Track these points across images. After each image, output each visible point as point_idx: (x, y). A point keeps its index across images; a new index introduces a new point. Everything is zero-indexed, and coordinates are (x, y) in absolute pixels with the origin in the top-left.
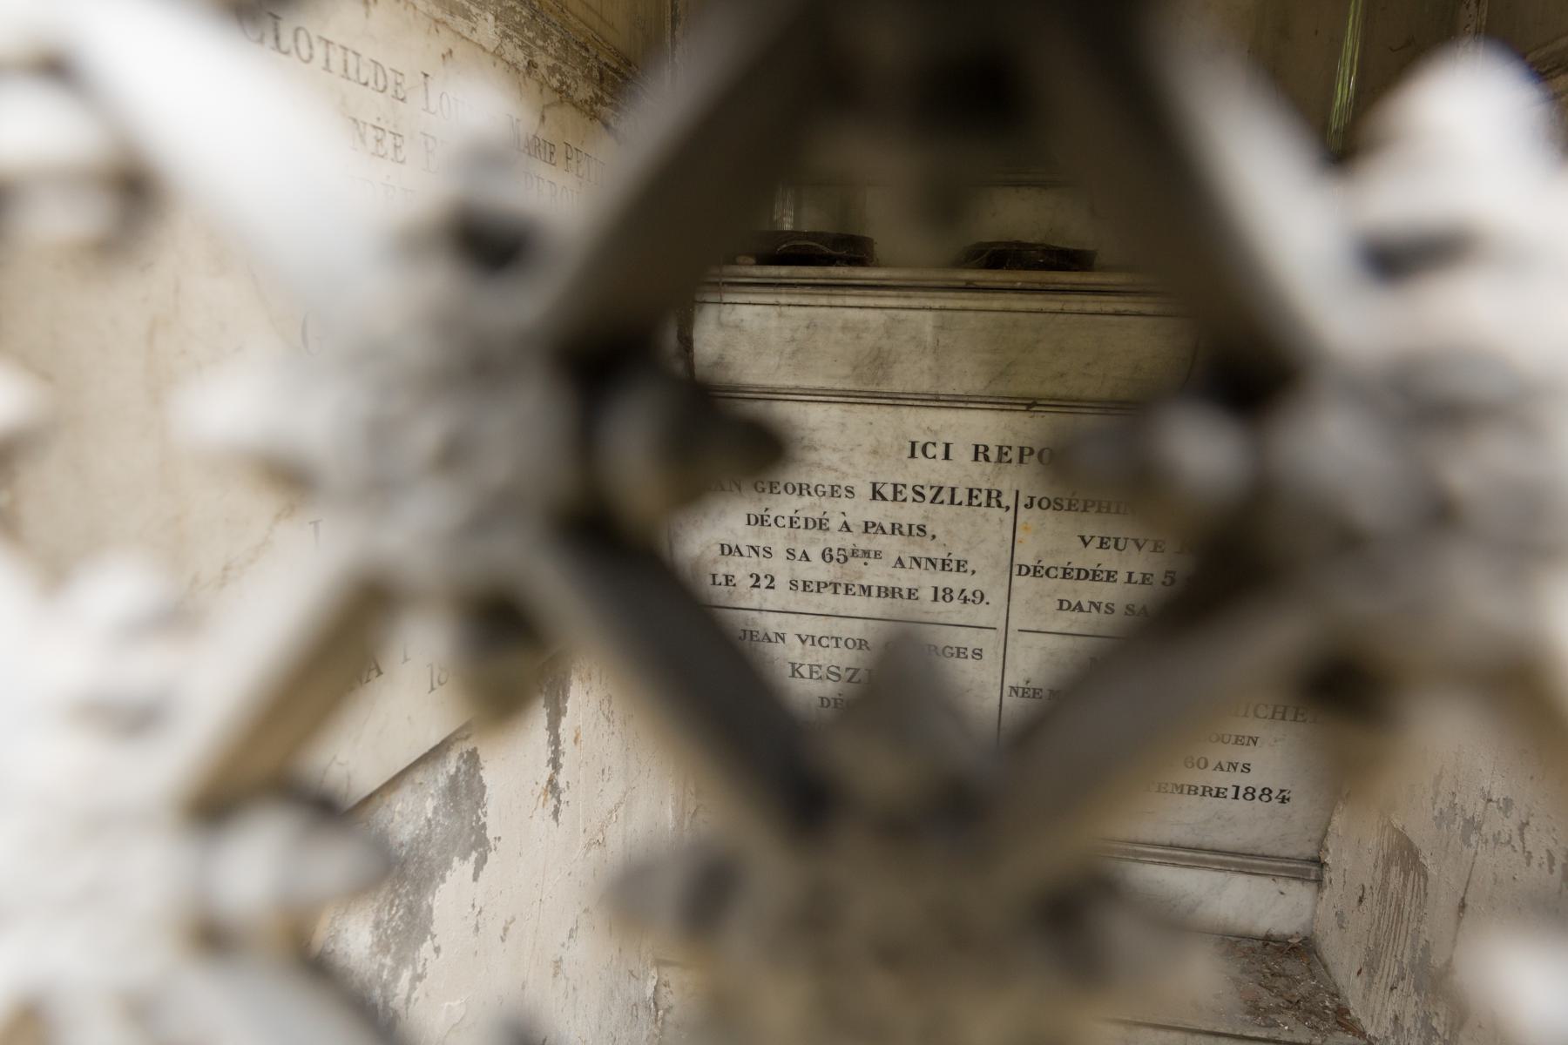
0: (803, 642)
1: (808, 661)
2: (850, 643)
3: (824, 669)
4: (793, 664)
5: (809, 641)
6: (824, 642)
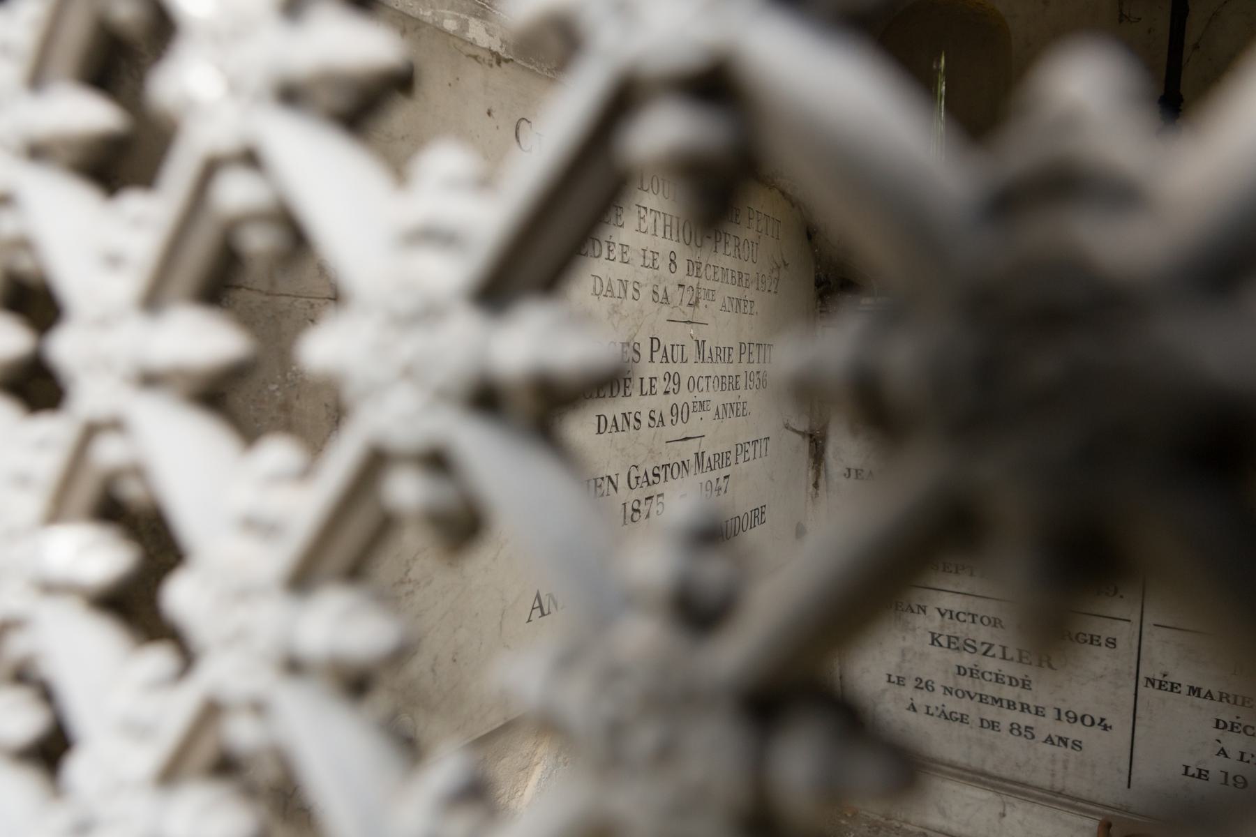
0: (942, 615)
1: (947, 632)
2: (985, 621)
3: (961, 641)
4: (933, 634)
5: (948, 615)
6: (962, 617)
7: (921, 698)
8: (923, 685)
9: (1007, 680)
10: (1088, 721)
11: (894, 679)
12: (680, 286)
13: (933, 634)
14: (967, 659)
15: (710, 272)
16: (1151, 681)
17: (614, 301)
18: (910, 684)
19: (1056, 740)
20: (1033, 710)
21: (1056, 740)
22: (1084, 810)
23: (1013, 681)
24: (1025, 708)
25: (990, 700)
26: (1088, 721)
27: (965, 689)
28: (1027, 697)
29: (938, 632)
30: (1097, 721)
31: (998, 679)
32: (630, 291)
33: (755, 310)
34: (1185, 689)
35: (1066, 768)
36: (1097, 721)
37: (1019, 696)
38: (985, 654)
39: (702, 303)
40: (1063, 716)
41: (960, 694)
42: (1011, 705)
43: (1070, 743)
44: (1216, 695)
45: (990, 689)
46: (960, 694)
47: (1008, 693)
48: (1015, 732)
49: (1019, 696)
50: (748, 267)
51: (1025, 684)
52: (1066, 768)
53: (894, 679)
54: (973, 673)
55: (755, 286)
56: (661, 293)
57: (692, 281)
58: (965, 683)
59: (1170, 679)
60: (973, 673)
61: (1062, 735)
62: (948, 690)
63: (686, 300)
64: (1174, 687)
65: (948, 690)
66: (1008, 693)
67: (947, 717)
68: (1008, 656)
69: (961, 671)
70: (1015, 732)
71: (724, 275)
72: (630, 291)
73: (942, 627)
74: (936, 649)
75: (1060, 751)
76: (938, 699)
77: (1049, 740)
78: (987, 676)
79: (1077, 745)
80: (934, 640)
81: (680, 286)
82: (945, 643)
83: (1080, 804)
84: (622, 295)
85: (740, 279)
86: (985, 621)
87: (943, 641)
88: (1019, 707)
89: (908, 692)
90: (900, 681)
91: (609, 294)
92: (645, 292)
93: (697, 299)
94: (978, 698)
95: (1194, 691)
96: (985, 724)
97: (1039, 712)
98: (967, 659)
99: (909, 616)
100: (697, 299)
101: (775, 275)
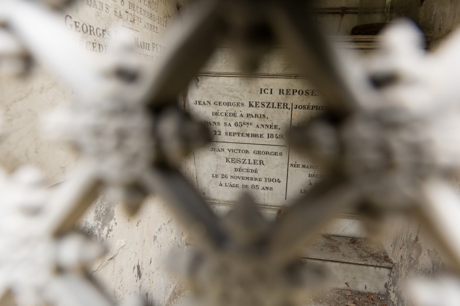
0: (230, 151)
1: (231, 157)
2: (243, 151)
3: (236, 159)
4: (227, 158)
5: (231, 151)
6: (236, 151)
7: (224, 181)
8: (224, 176)
9: (250, 171)
10: (274, 180)
11: (214, 176)
12: (126, 12)
13: (227, 158)
14: (238, 166)
15: (139, 10)
16: (292, 165)
17: (98, 10)
18: (220, 176)
19: (265, 188)
20: (258, 179)
21: (265, 188)
22: (273, 209)
23: (252, 171)
24: (256, 179)
25: (245, 178)
26: (274, 180)
27: (237, 176)
28: (256, 176)
29: (228, 157)
30: (277, 180)
31: (248, 171)
32: (104, 8)
33: (158, 31)
34: (301, 166)
35: (268, 197)
36: (277, 180)
37: (254, 176)
38: (245, 160)
39: (136, 22)
40: (267, 180)
41: (236, 178)
42: (252, 179)
43: (269, 189)
44: (309, 167)
45: (245, 175)
46: (236, 178)
47: (251, 175)
48: (253, 188)
49: (254, 176)
50: (154, 13)
51: (256, 171)
52: (268, 197)
53: (214, 176)
54: (240, 170)
55: (157, 21)
56: (118, 12)
57: (131, 11)
58: (237, 174)
59: (297, 163)
60: (240, 170)
61: (267, 186)
62: (232, 177)
63: (129, 19)
64: (298, 166)
65: (232, 177)
66: (251, 175)
67: (232, 186)
68: (251, 163)
69: (236, 170)
70: (253, 188)
71: (145, 13)
72: (104, 8)
73: (230, 155)
74: (228, 163)
75: (266, 192)
76: (229, 181)
77: (263, 188)
78: (244, 170)
79: (271, 189)
80: (227, 160)
81: (126, 12)
82: (231, 161)
83: (272, 207)
84: (101, 8)
85: (151, 16)
86: (243, 151)
87: (230, 160)
88: (254, 179)
89: (219, 179)
90: (217, 176)
91: (95, 6)
92: (111, 10)
93: (134, 20)
94: (241, 178)
95: (304, 166)
96: (244, 186)
97: (260, 180)
98: (238, 166)
99: (154, 300)
100: (134, 20)
101: (165, 19)
